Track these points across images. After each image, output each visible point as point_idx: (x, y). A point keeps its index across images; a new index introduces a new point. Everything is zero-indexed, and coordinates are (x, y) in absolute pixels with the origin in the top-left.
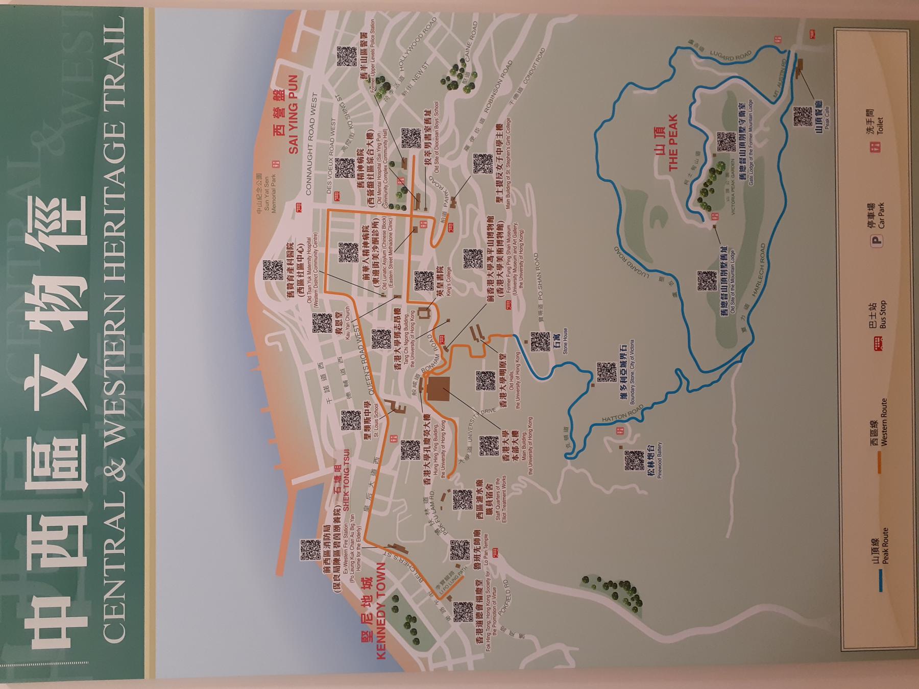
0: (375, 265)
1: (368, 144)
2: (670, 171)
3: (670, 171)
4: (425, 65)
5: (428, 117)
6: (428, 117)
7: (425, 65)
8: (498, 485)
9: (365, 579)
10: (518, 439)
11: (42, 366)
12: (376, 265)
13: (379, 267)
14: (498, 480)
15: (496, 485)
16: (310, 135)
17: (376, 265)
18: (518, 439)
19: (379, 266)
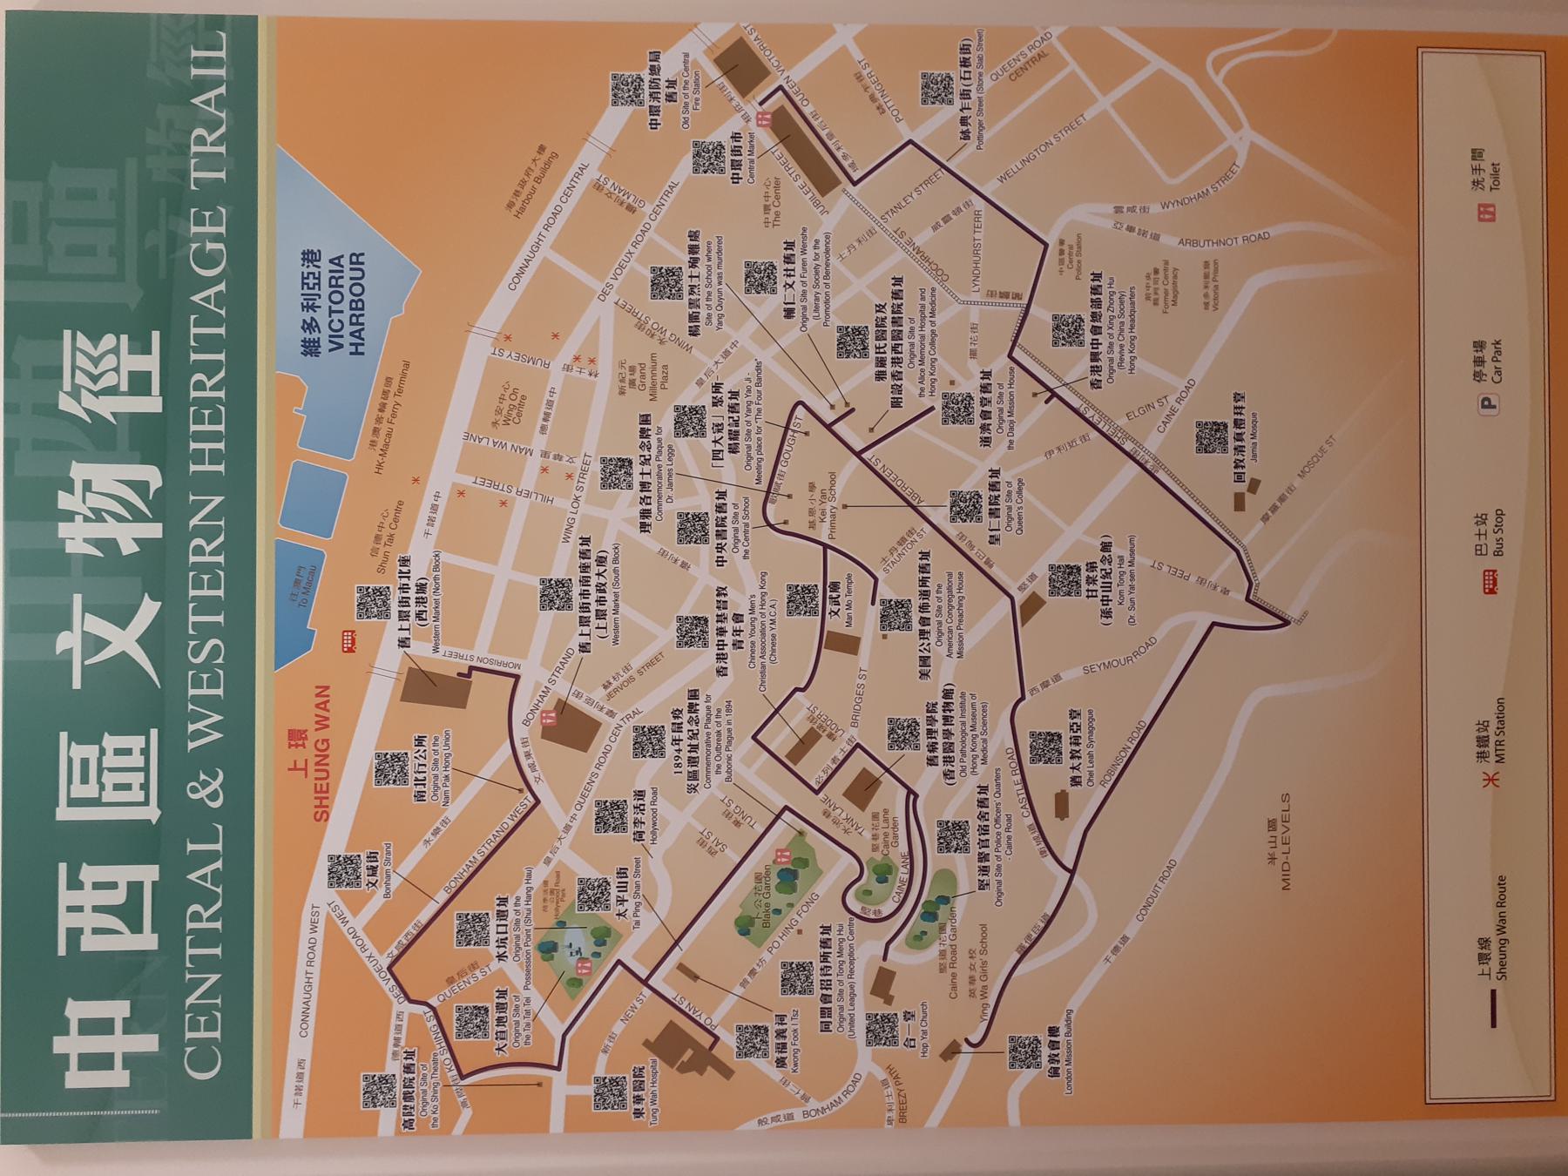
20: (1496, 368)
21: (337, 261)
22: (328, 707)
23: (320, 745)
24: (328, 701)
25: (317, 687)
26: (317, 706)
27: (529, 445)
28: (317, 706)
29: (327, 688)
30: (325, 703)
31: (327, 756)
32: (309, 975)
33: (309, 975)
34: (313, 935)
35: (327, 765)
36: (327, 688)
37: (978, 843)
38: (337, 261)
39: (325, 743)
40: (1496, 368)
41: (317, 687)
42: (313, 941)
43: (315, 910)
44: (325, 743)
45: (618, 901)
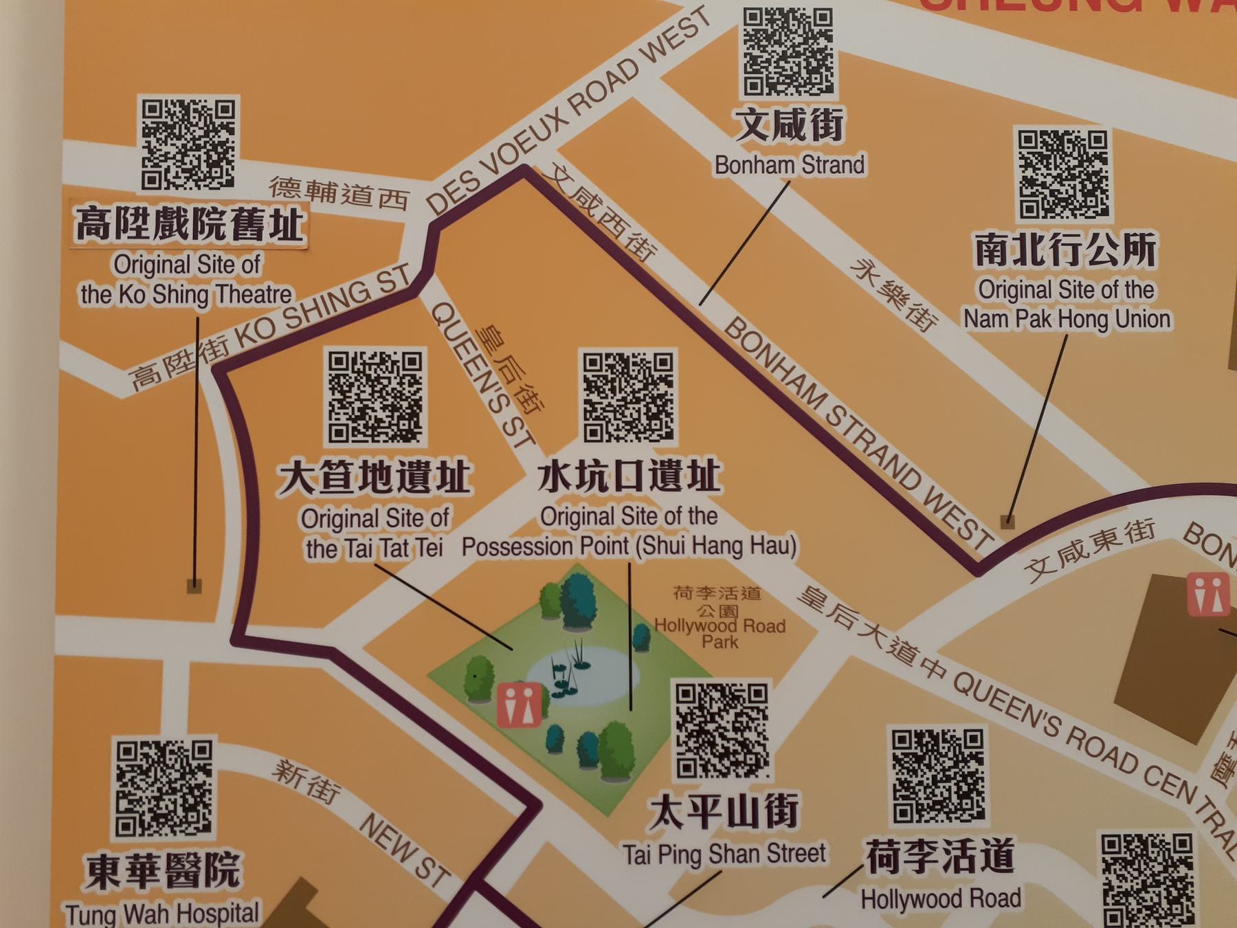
0: (826, 120)
1: (297, 471)
2: (704, 646)
3: (704, 646)
4: (435, 873)
5: (268, 225)
6: (268, 225)
7: (435, 873)
8: (1122, 289)
9: (800, 116)
10: (310, 490)
11: (556, 673)
12: (827, 128)
13: (816, 138)
14: (1146, 292)
15: (1122, 284)
16: (766, 631)
17: (827, 128)
18: (310, 490)
19: (822, 141)
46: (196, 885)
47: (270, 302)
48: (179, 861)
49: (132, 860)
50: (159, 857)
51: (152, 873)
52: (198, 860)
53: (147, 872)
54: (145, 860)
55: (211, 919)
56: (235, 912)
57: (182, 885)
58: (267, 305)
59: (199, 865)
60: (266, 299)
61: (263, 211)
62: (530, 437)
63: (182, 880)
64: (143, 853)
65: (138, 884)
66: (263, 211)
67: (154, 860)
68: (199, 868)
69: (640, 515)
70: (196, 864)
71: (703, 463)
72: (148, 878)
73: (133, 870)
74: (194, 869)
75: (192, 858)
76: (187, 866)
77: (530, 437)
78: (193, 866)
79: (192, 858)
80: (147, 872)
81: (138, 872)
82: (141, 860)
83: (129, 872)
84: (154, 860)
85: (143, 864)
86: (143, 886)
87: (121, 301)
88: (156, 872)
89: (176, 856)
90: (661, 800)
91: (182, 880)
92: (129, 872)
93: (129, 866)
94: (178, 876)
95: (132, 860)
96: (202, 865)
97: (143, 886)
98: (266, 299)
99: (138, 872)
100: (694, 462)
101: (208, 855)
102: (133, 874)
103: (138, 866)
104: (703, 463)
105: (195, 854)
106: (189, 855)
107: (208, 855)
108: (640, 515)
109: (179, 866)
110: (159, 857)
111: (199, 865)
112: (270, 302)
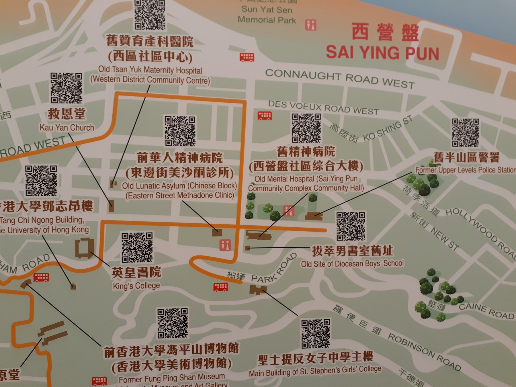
20: (455, 169)
21: (343, 52)
22: (342, 57)
23: (393, 51)
24: (347, 57)
25: (437, 49)
26: (343, 48)
27: (198, 138)
28: (343, 48)
29: (437, 58)
30: (346, 54)
31: (384, 57)
32: (336, 76)
33: (336, 76)
34: (381, 82)
35: (430, 58)
36: (437, 58)
37: (364, 246)
38: (343, 52)
39: (395, 56)
40: (455, 169)
41: (437, 49)
42: (375, 81)
43: (409, 85)
44: (395, 56)
45: (184, 346)
46: (180, 46)
47: (154, 188)
48: (174, 39)
49: (151, 154)
50: (160, 153)
51: (158, 158)
52: (180, 39)
53: (157, 158)
54: (156, 154)
55: (187, 72)
56: (195, 70)
57: (175, 46)
58: (153, 189)
59: (181, 40)
60: (154, 71)
61: (117, 36)
62: (377, 110)
63: (175, 44)
64: (155, 152)
65: (154, 161)
66: (117, 36)
67: (159, 154)
68: (180, 41)
69: (320, 264)
70: (180, 40)
71: (387, 247)
72: (157, 160)
73: (152, 157)
74: (179, 41)
75: (178, 38)
76: (177, 40)
77: (377, 110)
78: (179, 40)
79: (178, 38)
80: (157, 158)
81: (154, 158)
82: (155, 154)
83: (151, 158)
84: (159, 154)
85: (155, 155)
86: (155, 162)
87: (41, 130)
88: (159, 158)
89: (173, 37)
90: (340, 162)
91: (175, 44)
92: (151, 158)
93: (151, 156)
94: (174, 43)
95: (151, 154)
96: (182, 40)
97: (155, 162)
98: (154, 71)
99: (154, 158)
100: (385, 246)
101: (183, 37)
102: (152, 158)
103: (154, 156)
104: (387, 247)
105: (179, 37)
106: (177, 37)
107: (183, 37)
108: (320, 264)
109: (174, 40)
110: (160, 153)
111: (181, 40)
112: (154, 188)
